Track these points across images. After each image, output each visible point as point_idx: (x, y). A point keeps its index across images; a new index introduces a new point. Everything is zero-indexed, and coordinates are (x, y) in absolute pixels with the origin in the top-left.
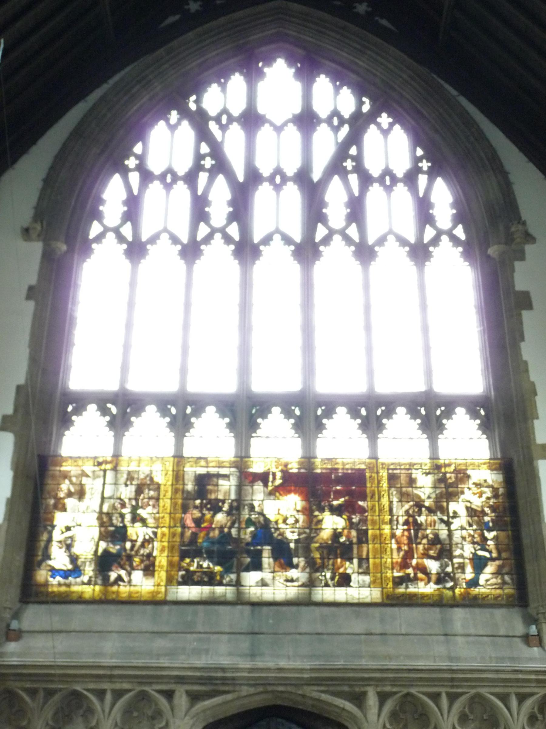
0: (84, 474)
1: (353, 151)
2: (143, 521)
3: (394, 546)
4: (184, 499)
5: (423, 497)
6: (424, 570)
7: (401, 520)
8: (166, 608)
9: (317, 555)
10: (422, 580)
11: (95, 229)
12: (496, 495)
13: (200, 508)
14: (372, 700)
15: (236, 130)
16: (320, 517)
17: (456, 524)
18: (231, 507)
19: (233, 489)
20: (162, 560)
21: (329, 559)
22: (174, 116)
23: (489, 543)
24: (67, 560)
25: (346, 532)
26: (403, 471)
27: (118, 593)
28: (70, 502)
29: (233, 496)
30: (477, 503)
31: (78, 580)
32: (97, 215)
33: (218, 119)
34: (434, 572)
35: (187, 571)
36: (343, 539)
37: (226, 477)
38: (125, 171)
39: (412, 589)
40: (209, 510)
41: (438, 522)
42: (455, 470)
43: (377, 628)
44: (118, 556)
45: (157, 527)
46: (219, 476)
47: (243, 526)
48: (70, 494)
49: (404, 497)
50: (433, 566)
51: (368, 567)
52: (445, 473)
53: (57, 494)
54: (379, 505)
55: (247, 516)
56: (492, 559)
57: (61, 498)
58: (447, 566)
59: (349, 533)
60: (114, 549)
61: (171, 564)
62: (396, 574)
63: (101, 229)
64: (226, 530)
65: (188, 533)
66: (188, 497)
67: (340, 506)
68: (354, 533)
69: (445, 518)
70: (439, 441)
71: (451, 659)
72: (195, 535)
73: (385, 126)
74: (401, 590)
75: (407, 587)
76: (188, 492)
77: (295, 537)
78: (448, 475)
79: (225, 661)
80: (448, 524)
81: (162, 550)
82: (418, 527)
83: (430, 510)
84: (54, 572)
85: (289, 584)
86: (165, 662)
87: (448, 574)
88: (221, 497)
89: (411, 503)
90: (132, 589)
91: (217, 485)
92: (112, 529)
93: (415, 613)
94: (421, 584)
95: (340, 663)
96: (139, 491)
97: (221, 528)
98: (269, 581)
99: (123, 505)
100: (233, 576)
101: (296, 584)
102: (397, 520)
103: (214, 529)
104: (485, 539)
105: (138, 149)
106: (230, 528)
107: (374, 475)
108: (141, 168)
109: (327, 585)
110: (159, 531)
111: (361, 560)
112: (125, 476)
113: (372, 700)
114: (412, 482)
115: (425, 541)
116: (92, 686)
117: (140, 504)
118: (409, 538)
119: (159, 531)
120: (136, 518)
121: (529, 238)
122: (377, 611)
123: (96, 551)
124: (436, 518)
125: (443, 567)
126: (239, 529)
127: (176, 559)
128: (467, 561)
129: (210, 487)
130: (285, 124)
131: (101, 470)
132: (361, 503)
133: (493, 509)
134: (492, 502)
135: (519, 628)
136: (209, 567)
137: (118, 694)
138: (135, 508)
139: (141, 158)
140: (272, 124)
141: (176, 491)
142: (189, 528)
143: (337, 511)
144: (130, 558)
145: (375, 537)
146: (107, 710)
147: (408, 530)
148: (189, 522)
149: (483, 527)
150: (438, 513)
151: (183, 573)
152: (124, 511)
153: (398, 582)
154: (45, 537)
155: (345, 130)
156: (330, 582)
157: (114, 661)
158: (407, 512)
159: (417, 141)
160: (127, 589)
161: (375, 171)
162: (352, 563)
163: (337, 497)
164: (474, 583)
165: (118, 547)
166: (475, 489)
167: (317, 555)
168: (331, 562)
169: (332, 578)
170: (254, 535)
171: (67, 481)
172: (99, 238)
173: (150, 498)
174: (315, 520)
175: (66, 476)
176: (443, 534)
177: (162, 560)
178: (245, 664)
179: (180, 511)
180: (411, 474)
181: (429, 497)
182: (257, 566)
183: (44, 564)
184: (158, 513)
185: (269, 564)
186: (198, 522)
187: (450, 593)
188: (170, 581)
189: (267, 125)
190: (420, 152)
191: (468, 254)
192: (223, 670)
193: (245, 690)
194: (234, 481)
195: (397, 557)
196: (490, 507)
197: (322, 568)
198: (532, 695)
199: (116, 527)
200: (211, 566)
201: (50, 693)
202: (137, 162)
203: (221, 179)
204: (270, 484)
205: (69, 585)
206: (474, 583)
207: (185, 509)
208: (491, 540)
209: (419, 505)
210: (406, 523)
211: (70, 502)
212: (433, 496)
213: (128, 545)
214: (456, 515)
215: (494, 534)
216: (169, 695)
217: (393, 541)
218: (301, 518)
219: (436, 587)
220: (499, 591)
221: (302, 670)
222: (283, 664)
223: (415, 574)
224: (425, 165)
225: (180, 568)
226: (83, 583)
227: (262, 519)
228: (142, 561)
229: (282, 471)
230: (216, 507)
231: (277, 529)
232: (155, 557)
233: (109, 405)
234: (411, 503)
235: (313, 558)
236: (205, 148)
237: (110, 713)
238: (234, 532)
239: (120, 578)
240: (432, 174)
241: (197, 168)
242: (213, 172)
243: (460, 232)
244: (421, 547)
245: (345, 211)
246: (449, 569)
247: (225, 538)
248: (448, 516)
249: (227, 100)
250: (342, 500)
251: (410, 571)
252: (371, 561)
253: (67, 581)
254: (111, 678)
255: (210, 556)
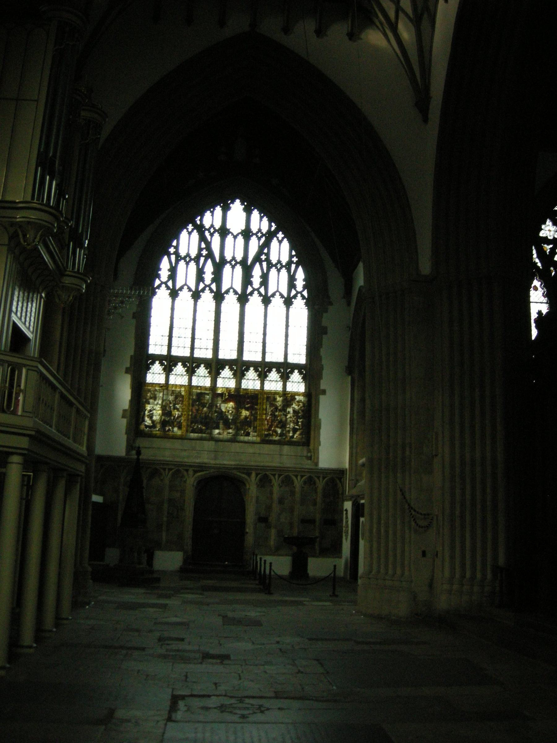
0: (156, 390)
1: (266, 251)
2: (178, 410)
3: (266, 423)
4: (192, 402)
5: (278, 405)
6: (276, 432)
7: (269, 413)
8: (186, 441)
9: (239, 425)
10: (274, 435)
11: (157, 282)
12: (304, 406)
13: (198, 405)
14: (253, 475)
15: (217, 236)
16: (241, 411)
17: (289, 416)
18: (209, 405)
19: (210, 399)
20: (184, 424)
21: (243, 426)
22: (190, 227)
23: (300, 423)
24: (150, 422)
25: (250, 417)
26: (272, 395)
27: (169, 435)
28: (151, 401)
29: (210, 402)
30: (297, 408)
31: (155, 429)
32: (159, 276)
33: (209, 230)
34: (279, 432)
35: (193, 428)
36: (248, 420)
37: (208, 394)
38: (169, 255)
39: (271, 438)
40: (201, 406)
41: (282, 415)
42: (291, 396)
43: (258, 451)
44: (168, 422)
45: (183, 412)
46: (205, 394)
47: (213, 413)
48: (151, 398)
49: (272, 405)
50: (279, 431)
51: (256, 430)
52: (287, 397)
53: (146, 398)
54: (262, 408)
55: (215, 409)
56: (299, 429)
57: (148, 399)
58: (284, 431)
59: (251, 417)
60: (167, 419)
61: (188, 425)
62: (266, 433)
63: (160, 282)
64: (207, 414)
65: (194, 414)
66: (194, 401)
67: (249, 407)
68: (252, 417)
69: (285, 414)
70: (290, 309)
71: (281, 463)
72: (196, 415)
73: (280, 239)
74: (267, 438)
75: (269, 438)
76: (194, 400)
77: (232, 418)
78: (288, 398)
79: (206, 461)
80: (286, 416)
81: (184, 420)
82: (276, 416)
83: (280, 411)
84: (146, 426)
85: (229, 435)
86: (186, 460)
87: (284, 434)
88: (206, 402)
89: (274, 408)
90: (174, 433)
91: (204, 397)
92: (166, 411)
93: (272, 447)
94: (274, 437)
95: (244, 463)
96: (176, 398)
97: (206, 413)
98: (222, 433)
99: (170, 403)
100: (209, 431)
101: (231, 435)
102: (268, 413)
103: (203, 414)
104: (298, 422)
105: (174, 243)
106: (209, 414)
107: (262, 396)
108: (177, 253)
109: (242, 436)
110: (183, 413)
111: (254, 428)
112: (171, 392)
113: (253, 475)
114: (275, 399)
115: (277, 422)
116: (161, 466)
117: (177, 403)
118: (272, 420)
119: (183, 413)
120: (175, 408)
121: (331, 304)
122: (258, 445)
123: (161, 419)
124: (282, 413)
125: (282, 431)
126: (212, 414)
127: (189, 424)
128: (291, 429)
129: (202, 398)
130: (238, 235)
131: (162, 389)
132: (256, 407)
133: (303, 411)
134: (302, 408)
135: (305, 453)
136: (201, 427)
137: (170, 470)
138: (174, 405)
139: (177, 247)
140: (232, 234)
141: (189, 399)
142: (194, 413)
143: (247, 409)
144: (173, 423)
145: (260, 419)
146: (166, 474)
147: (272, 417)
148: (194, 411)
149: (298, 417)
150: (283, 412)
151: (191, 429)
152: (171, 405)
153: (267, 435)
154: (142, 413)
155: (263, 239)
156: (243, 435)
157: (168, 459)
158: (272, 411)
159: (292, 248)
160: (172, 433)
161: (274, 261)
162: (251, 428)
163: (248, 403)
164: (292, 437)
165: (168, 418)
166: (297, 404)
167: (239, 425)
168: (244, 427)
169: (244, 433)
170: (217, 416)
171: (150, 393)
172: (159, 287)
173: (180, 401)
174: (239, 412)
175: (149, 391)
176: (284, 419)
177: (184, 424)
178: (213, 462)
179: (191, 406)
180: (275, 397)
181: (280, 406)
182: (218, 428)
183: (142, 423)
184: (183, 406)
185: (222, 427)
186: (197, 410)
187: (284, 440)
188: (187, 431)
189: (230, 234)
190: (294, 253)
191: (307, 304)
192: (206, 464)
193: (212, 471)
194: (210, 395)
195: (267, 427)
196: (301, 410)
197: (241, 429)
198: (305, 476)
199: (168, 411)
200: (202, 427)
201: (170, 470)
202: (175, 250)
203: (209, 262)
204: (224, 398)
205: (151, 431)
206: (292, 437)
207: (193, 405)
208: (300, 422)
209: (276, 408)
210: (271, 415)
211: (151, 401)
212: (282, 405)
213: (172, 418)
214: (289, 412)
215: (301, 420)
216: (187, 471)
217: (266, 421)
218: (234, 411)
219: (280, 438)
220: (300, 440)
221: (231, 465)
222: (225, 462)
223: (273, 433)
224: (295, 259)
225: (191, 427)
226: (157, 431)
227: (220, 411)
228: (177, 424)
229: (228, 393)
230: (204, 406)
231: (225, 415)
232: (182, 423)
233: (164, 362)
234: (274, 408)
235: (238, 426)
236: (203, 245)
237: (168, 475)
238: (210, 415)
239: (169, 430)
240: (297, 264)
241: (199, 255)
242: (207, 257)
243: (305, 293)
244: (275, 424)
245: (260, 280)
246: (284, 432)
247: (206, 417)
248: (286, 413)
249: (214, 221)
250: (249, 405)
251: (271, 432)
252: (258, 428)
253: (151, 430)
254: (168, 464)
255: (201, 423)
